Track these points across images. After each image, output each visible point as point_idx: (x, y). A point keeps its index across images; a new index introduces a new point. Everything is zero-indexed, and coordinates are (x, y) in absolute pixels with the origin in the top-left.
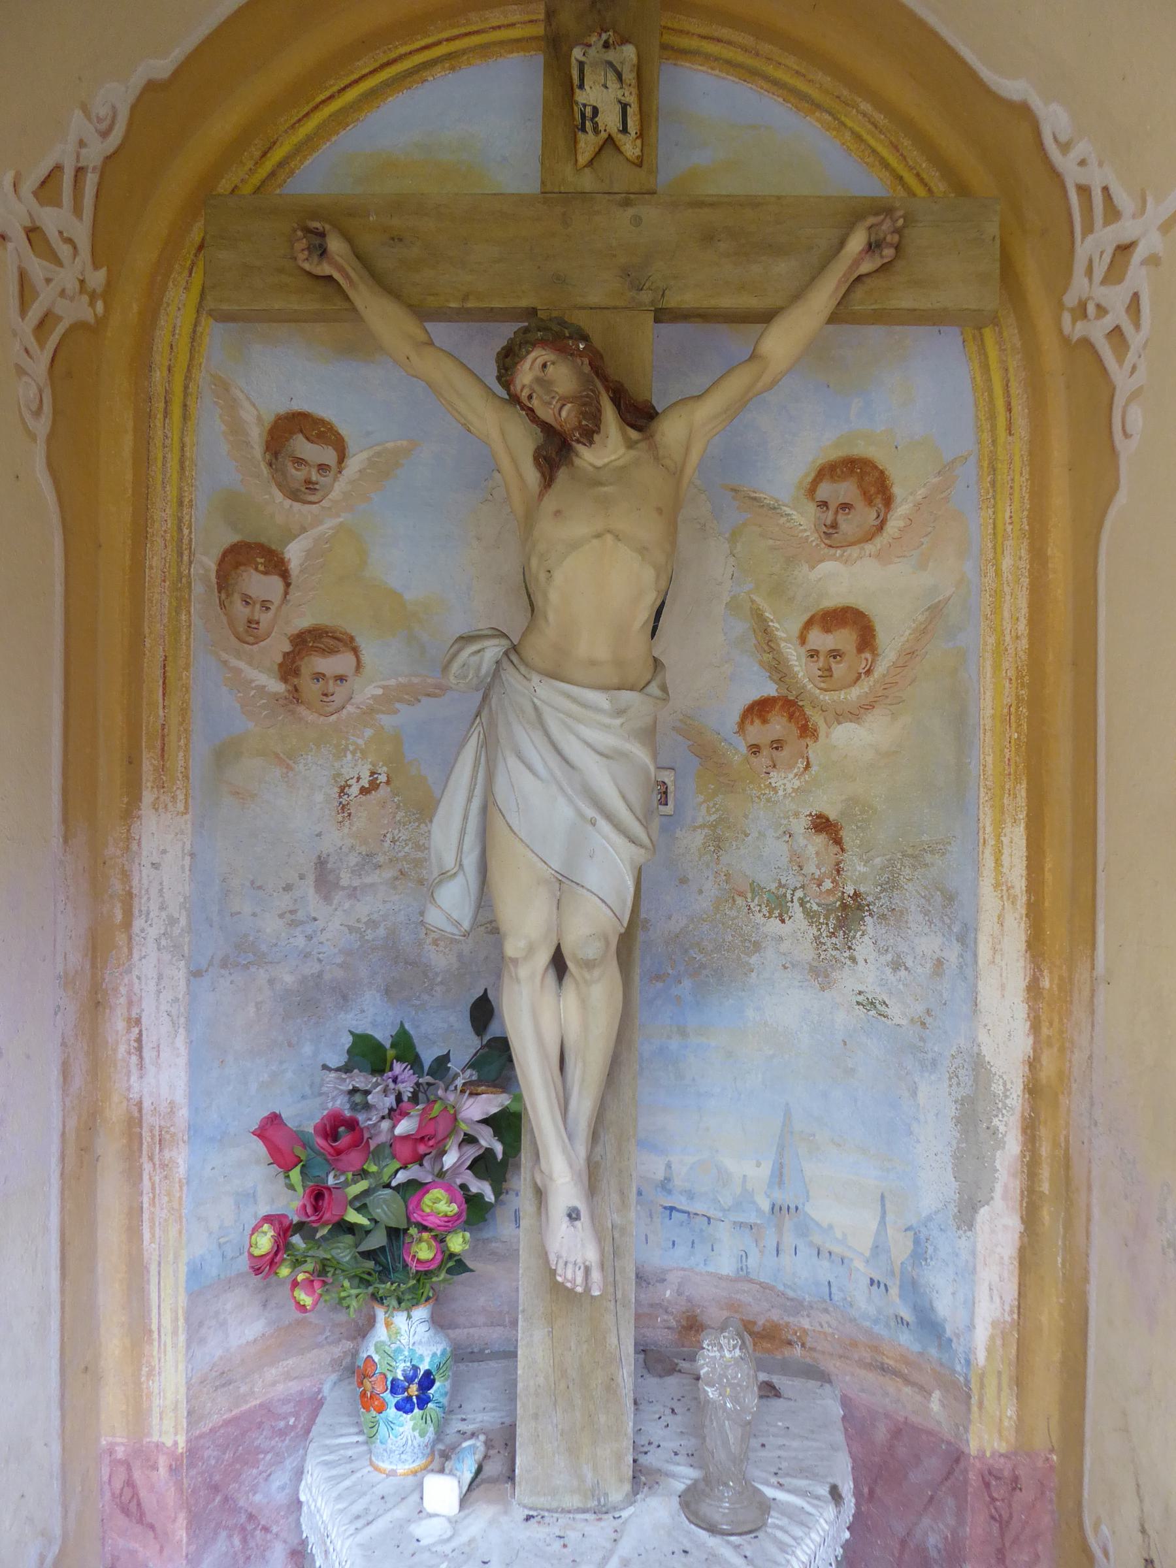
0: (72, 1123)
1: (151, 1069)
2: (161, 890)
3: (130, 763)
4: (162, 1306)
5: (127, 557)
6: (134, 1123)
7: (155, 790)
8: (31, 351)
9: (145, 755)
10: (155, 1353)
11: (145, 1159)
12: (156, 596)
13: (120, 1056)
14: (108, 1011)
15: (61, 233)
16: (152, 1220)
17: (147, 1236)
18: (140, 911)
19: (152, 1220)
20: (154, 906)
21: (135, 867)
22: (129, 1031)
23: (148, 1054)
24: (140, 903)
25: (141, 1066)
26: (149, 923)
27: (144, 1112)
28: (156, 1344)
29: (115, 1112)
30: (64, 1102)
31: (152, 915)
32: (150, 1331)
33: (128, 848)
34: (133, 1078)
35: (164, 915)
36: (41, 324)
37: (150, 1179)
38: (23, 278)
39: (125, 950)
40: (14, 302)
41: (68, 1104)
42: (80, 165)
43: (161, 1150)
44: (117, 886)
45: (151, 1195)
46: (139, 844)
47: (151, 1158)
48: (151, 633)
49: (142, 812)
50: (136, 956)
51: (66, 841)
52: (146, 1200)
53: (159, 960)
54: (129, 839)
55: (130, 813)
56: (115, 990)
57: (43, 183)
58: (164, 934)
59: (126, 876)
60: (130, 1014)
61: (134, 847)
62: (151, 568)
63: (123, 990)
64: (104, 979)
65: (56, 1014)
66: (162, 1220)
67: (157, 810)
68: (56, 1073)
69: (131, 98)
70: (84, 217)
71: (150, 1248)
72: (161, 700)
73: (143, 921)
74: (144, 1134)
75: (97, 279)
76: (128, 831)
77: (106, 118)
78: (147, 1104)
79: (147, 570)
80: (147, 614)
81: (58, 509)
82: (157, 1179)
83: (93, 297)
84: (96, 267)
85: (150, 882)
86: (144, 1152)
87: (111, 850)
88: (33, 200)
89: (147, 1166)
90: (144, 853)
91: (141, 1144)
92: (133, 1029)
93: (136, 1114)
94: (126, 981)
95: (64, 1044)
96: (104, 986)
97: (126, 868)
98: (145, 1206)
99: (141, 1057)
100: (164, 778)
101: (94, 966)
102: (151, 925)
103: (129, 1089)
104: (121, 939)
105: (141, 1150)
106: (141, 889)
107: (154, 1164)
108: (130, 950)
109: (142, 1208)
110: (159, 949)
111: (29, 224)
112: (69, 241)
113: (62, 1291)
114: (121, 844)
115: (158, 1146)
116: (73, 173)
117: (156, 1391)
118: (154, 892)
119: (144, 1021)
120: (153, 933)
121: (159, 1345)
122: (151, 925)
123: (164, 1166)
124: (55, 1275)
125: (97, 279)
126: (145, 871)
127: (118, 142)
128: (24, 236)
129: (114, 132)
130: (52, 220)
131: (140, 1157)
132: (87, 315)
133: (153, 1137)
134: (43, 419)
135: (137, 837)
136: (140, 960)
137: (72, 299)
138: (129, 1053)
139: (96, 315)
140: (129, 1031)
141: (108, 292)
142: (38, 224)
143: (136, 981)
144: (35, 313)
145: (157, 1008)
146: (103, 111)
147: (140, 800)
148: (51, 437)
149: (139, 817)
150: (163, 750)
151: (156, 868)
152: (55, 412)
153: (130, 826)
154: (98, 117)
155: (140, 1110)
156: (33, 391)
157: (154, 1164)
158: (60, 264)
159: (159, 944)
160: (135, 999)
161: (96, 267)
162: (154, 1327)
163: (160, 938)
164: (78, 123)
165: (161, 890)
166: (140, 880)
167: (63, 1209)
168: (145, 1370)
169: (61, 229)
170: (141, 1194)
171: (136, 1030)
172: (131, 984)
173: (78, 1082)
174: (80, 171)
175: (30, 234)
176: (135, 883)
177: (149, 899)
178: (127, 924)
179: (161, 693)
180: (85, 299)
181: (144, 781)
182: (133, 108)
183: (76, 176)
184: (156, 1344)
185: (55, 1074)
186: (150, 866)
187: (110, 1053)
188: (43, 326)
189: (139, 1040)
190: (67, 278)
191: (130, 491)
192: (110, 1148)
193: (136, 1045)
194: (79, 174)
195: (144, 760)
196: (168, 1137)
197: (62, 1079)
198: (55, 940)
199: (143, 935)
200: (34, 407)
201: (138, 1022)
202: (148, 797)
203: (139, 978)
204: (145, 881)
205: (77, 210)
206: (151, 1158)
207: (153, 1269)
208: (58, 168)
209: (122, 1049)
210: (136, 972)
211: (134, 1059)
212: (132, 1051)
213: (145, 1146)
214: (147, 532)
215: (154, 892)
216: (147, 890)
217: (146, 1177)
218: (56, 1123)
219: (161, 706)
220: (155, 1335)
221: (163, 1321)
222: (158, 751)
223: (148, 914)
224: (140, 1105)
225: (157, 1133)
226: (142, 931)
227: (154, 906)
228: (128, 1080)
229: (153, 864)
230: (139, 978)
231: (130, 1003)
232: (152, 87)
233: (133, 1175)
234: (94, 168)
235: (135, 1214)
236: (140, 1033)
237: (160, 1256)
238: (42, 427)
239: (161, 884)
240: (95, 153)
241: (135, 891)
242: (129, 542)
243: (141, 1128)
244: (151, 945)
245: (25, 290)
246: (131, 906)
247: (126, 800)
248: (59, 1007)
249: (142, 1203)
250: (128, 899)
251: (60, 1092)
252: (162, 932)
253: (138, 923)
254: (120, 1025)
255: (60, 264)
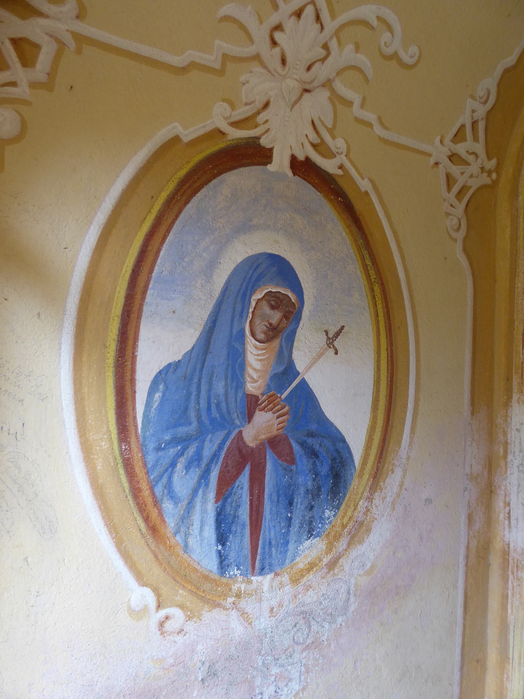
0: (474, 543)
1: (514, 530)
2: (520, 443)
3: (508, 380)
4: (515, 648)
5: (508, 284)
6: (506, 553)
7: (518, 393)
8: (454, 204)
9: (514, 376)
10: (510, 669)
11: (510, 572)
12: (520, 301)
13: (501, 519)
14: (496, 496)
15: (467, 152)
16: (512, 604)
17: (509, 611)
18: (511, 451)
19: (512, 604)
20: (517, 450)
21: (509, 430)
22: (505, 508)
23: (513, 522)
24: (511, 447)
25: (510, 526)
26: (515, 458)
27: (511, 549)
28: (511, 665)
29: (498, 545)
30: (469, 533)
31: (516, 454)
32: (509, 658)
33: (506, 421)
34: (506, 532)
35: (521, 455)
36: (460, 192)
37: (512, 583)
38: (448, 176)
39: (504, 469)
40: (444, 188)
41: (471, 534)
42: (474, 120)
43: (517, 571)
44: (501, 438)
45: (512, 591)
46: (511, 419)
47: (513, 573)
48: (517, 319)
49: (512, 404)
50: (509, 473)
51: (473, 414)
52: (510, 593)
53: (518, 476)
54: (507, 416)
55: (507, 404)
56: (500, 487)
57: (456, 135)
58: (521, 464)
59: (505, 434)
60: (505, 500)
61: (509, 420)
62: (518, 288)
63: (503, 488)
64: (495, 481)
65: (464, 491)
66: (516, 606)
67: (519, 403)
68: (463, 517)
69: (496, 81)
70: (480, 140)
71: (511, 618)
72: (521, 350)
73: (512, 456)
74: (510, 560)
75: (492, 164)
76: (507, 412)
77: (484, 96)
78: (512, 546)
79: (516, 289)
80: (516, 310)
81: (469, 268)
82: (515, 584)
83: (489, 173)
84: (489, 158)
85: (516, 438)
86: (510, 569)
87: (499, 420)
88: (451, 144)
89: (511, 576)
90: (513, 424)
91: (508, 564)
92: (506, 508)
93: (507, 549)
94: (504, 484)
95: (469, 505)
96: (495, 484)
97: (505, 430)
98: (510, 595)
99: (510, 522)
100: (523, 388)
101: (490, 472)
102: (515, 459)
103: (504, 536)
104: (502, 463)
105: (508, 567)
106: (511, 440)
107: (514, 577)
108: (506, 469)
109: (508, 596)
110: (519, 471)
111: (449, 154)
112: (473, 153)
113: (465, 619)
114: (503, 418)
115: (516, 568)
116: (471, 125)
117: (510, 689)
118: (517, 442)
119: (511, 504)
120: (516, 462)
121: (512, 667)
122: (515, 459)
123: (518, 579)
124: (460, 611)
125: (492, 164)
126: (513, 433)
127: (493, 102)
128: (448, 160)
129: (490, 100)
130: (461, 149)
131: (508, 570)
132: (488, 181)
133: (514, 563)
134: (461, 232)
135: (510, 416)
136: (510, 475)
137: (477, 177)
138: (505, 519)
139: (492, 180)
140: (505, 508)
141: (498, 168)
142: (454, 152)
143: (508, 484)
144: (455, 189)
145: (517, 500)
146: (482, 94)
147: (512, 398)
148: (465, 239)
149: (511, 406)
150: (522, 374)
151: (518, 432)
152: (468, 228)
153: (507, 410)
154: (479, 97)
155: (509, 548)
156: (456, 221)
157: (514, 577)
158: (468, 164)
159: (519, 469)
160: (507, 493)
161: (489, 158)
162: (511, 657)
163: (519, 466)
164: (470, 104)
165: (520, 443)
166: (511, 437)
167: (466, 581)
168: (505, 676)
169: (467, 150)
170: (508, 589)
171: (508, 508)
172: (506, 486)
173: (477, 525)
174: (474, 124)
175: (452, 158)
176: (509, 437)
177: (515, 446)
178: (505, 457)
179: (521, 347)
180: (485, 174)
181: (513, 389)
182: (499, 85)
183: (473, 125)
184: (511, 665)
185: (463, 519)
186: (516, 430)
187: (496, 516)
188: (460, 195)
189: (509, 513)
190: (474, 169)
191: (509, 254)
192: (495, 561)
193: (507, 515)
194: (474, 124)
195: (514, 379)
196: (520, 565)
197: (467, 522)
198: (465, 458)
199: (512, 463)
200: (456, 228)
201: (509, 504)
202: (515, 397)
203: (510, 483)
204: (513, 437)
205: (476, 138)
206: (513, 573)
207: (511, 628)
208: (463, 126)
209: (502, 516)
210: (508, 480)
211: (507, 522)
212: (506, 518)
213: (510, 566)
214: (516, 271)
215: (517, 442)
216: (514, 442)
217: (510, 582)
218: (464, 540)
219: (521, 353)
220: (511, 661)
221: (515, 656)
222: (520, 375)
223: (514, 453)
224: (509, 545)
225: (516, 562)
226: (512, 461)
227: (517, 450)
228: (504, 532)
229: (517, 429)
230: (510, 483)
231: (506, 495)
232: (507, 71)
233: (505, 579)
234: (482, 119)
235: (505, 597)
236: (510, 510)
237: (515, 623)
238: (460, 235)
239: (520, 439)
240: (482, 111)
241: (509, 441)
242: (508, 277)
243: (509, 557)
244: (515, 470)
245: (450, 180)
246: (507, 448)
247: (505, 397)
248: (466, 488)
249: (508, 593)
250: (506, 444)
251: (467, 527)
252: (520, 463)
253: (510, 457)
254: (501, 504)
255: (468, 164)
